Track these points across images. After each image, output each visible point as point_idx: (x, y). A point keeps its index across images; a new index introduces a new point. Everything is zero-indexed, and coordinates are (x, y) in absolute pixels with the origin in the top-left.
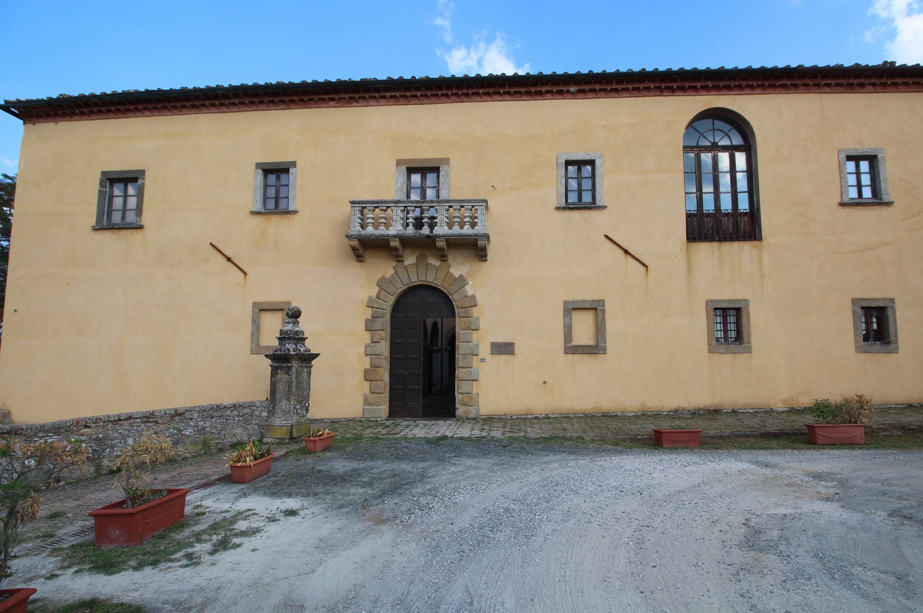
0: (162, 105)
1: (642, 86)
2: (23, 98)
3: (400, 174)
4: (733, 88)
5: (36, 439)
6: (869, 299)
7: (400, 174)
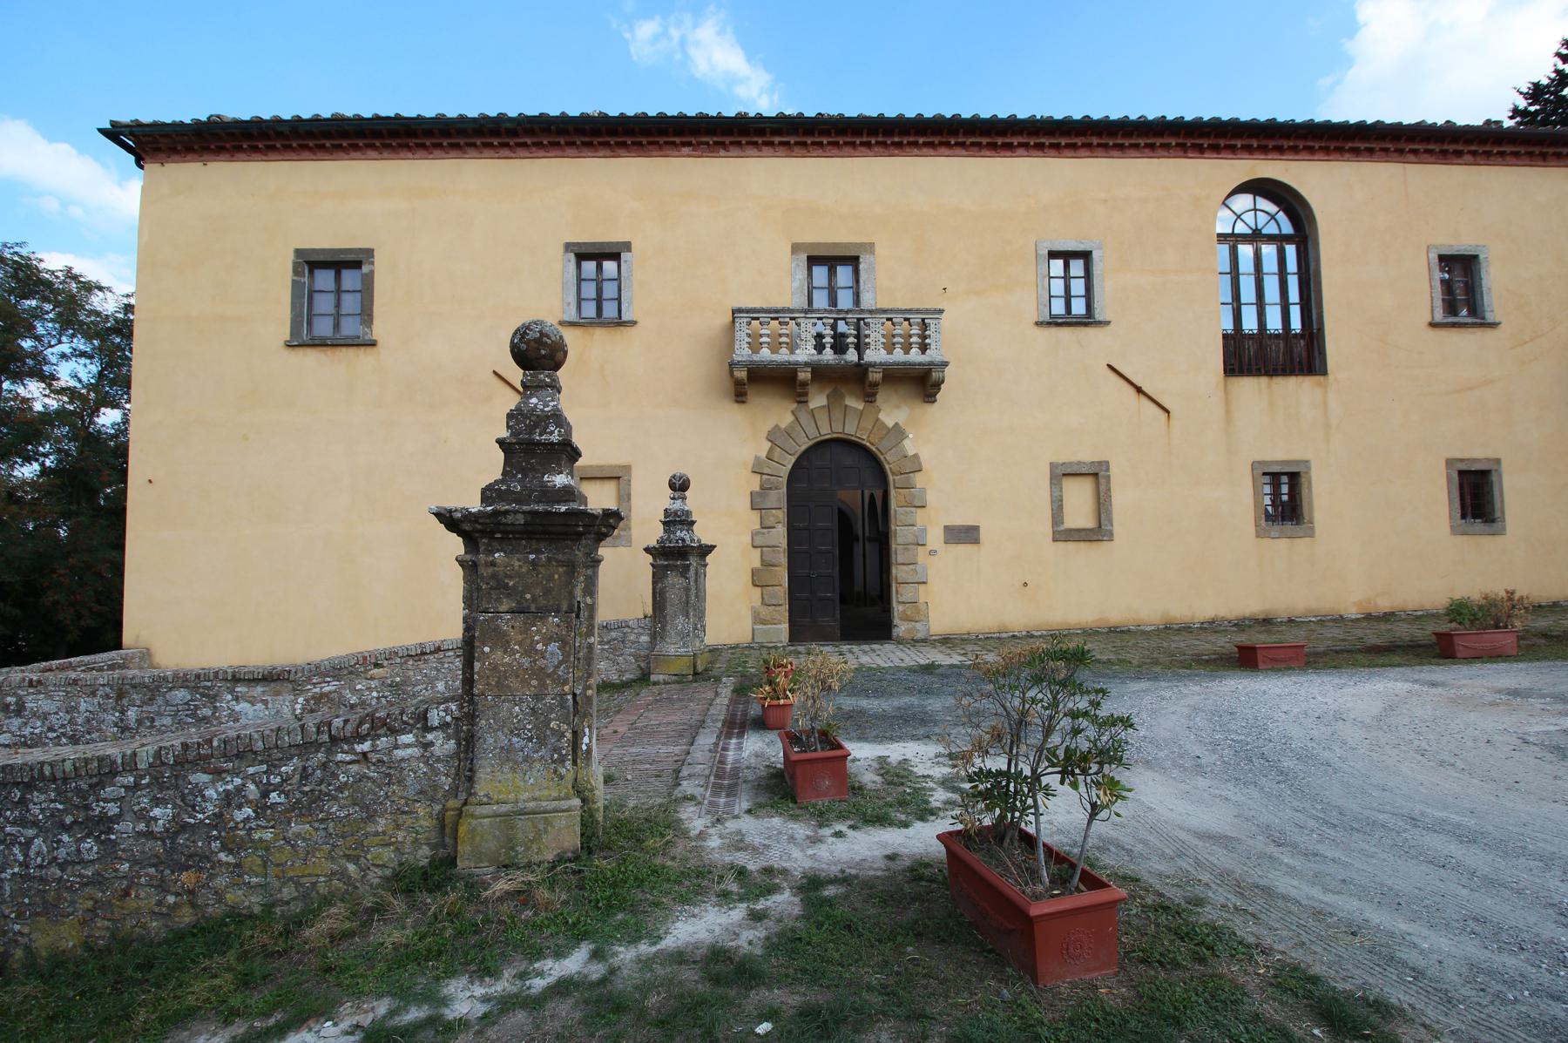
0: (569, 139)
1: (1158, 141)
2: (146, 119)
3: (798, 265)
4: (1300, 150)
5: (309, 687)
6: (1468, 460)
7: (798, 265)
